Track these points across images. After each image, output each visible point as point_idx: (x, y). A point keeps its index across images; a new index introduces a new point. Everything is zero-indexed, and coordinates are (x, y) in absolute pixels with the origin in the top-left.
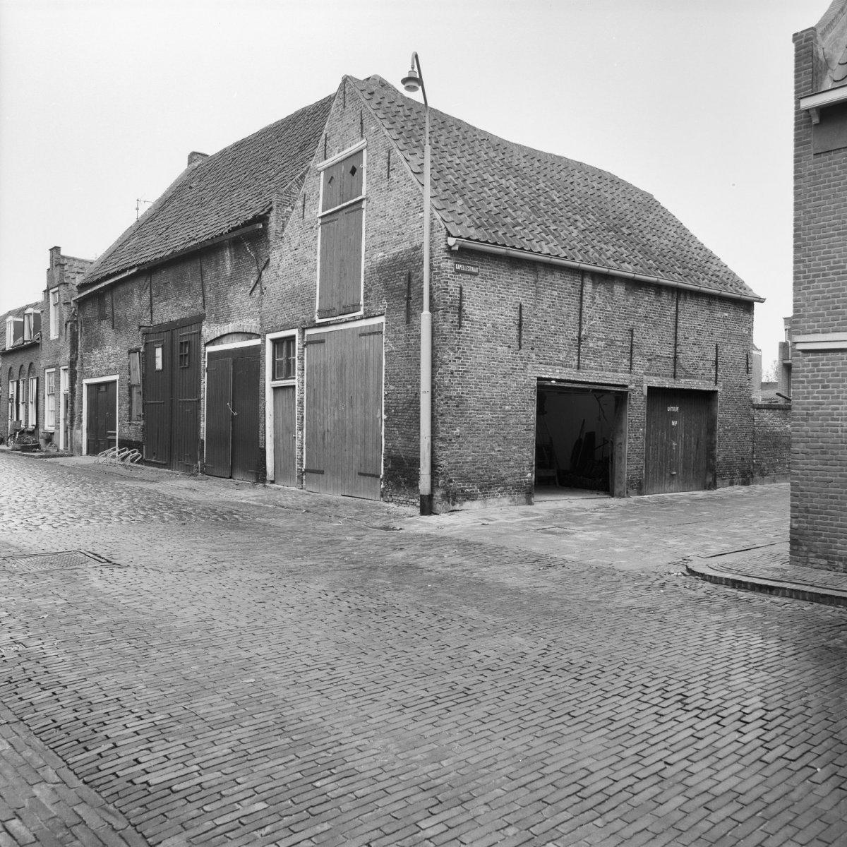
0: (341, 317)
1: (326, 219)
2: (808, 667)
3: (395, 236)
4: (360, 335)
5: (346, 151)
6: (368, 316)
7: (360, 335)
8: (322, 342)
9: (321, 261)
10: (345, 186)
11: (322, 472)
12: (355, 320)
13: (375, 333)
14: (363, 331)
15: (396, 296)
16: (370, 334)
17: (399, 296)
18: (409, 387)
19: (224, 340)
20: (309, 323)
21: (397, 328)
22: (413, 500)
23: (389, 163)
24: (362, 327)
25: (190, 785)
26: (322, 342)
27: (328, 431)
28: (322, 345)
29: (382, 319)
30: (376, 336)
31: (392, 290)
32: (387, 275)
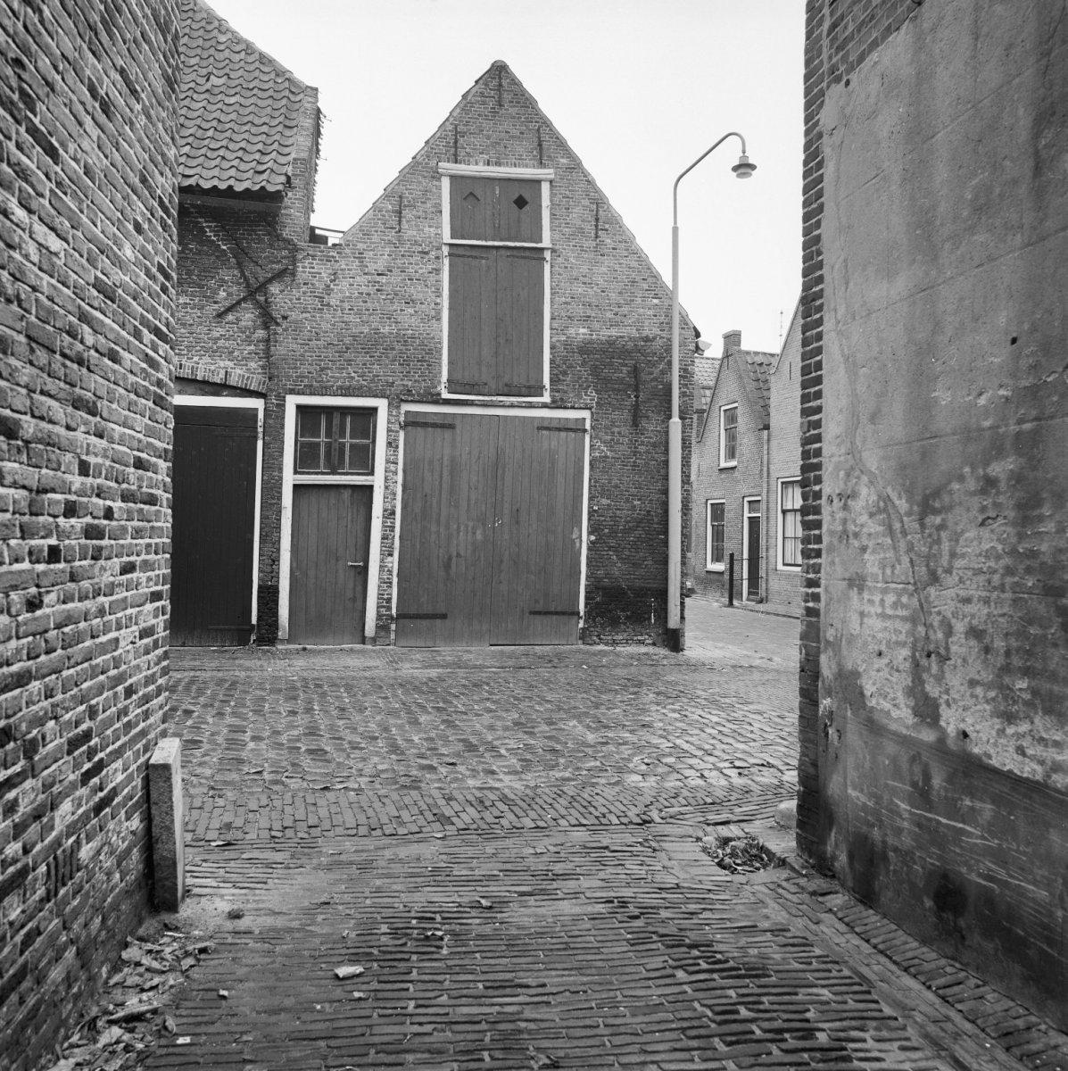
0: (501, 398)
1: (456, 251)
2: (731, 940)
3: (609, 315)
4: (539, 428)
5: (502, 169)
6: (556, 405)
7: (539, 428)
8: (451, 427)
9: (450, 309)
10: (168, 139)
11: (444, 617)
12: (531, 406)
13: (443, 426)
14: (546, 424)
15: (614, 390)
16: (559, 430)
17: (620, 391)
18: (636, 503)
19: (508, 404)
20: (423, 396)
21: (616, 430)
22: (639, 638)
23: (597, 220)
24: (543, 418)
25: (358, 1039)
26: (451, 427)
27: (458, 555)
28: (447, 434)
29: (586, 414)
30: (573, 435)
31: (607, 380)
32: (597, 360)
